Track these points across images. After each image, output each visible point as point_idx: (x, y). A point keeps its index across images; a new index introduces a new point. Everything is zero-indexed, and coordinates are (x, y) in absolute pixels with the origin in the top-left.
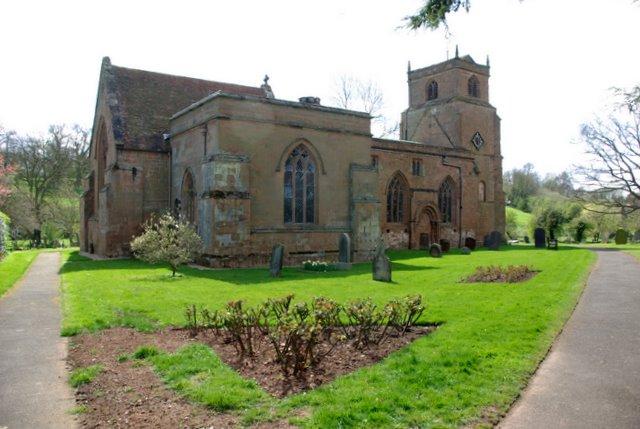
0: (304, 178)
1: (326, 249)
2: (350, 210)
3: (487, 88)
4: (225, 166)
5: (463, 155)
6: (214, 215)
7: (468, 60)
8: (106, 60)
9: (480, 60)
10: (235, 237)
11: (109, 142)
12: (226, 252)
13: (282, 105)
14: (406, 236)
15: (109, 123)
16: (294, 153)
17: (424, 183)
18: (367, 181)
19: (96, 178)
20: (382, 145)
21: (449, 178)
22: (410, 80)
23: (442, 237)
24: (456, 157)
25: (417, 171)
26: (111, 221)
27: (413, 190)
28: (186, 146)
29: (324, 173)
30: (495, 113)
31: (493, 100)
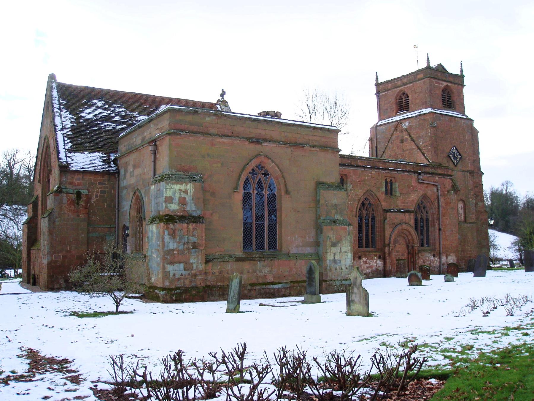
0: (265, 199)
1: (290, 279)
2: (317, 234)
3: (463, 99)
4: (177, 187)
5: (440, 172)
6: (163, 242)
7: (441, 69)
8: (52, 77)
9: (453, 69)
10: (188, 266)
11: (53, 164)
14: (380, 263)
17: (399, 203)
18: (335, 201)
19: (40, 203)
20: (350, 161)
21: (425, 196)
22: (378, 92)
23: (420, 262)
24: (433, 174)
25: (389, 191)
26: (53, 250)
27: (387, 211)
28: (135, 167)
29: (287, 192)
30: (472, 125)
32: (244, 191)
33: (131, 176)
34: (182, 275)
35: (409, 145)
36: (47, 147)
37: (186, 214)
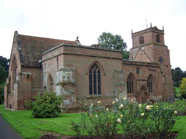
7: (155, 28)
8: (16, 32)
9: (160, 28)
10: (71, 101)
12: (68, 107)
13: (88, 48)
15: (18, 57)
16: (92, 67)
21: (151, 75)
22: (132, 37)
24: (153, 66)
30: (167, 48)
31: (166, 44)
32: (89, 74)
33: (48, 69)
34: (69, 104)
35: (144, 56)
36: (15, 57)
37: (70, 82)
